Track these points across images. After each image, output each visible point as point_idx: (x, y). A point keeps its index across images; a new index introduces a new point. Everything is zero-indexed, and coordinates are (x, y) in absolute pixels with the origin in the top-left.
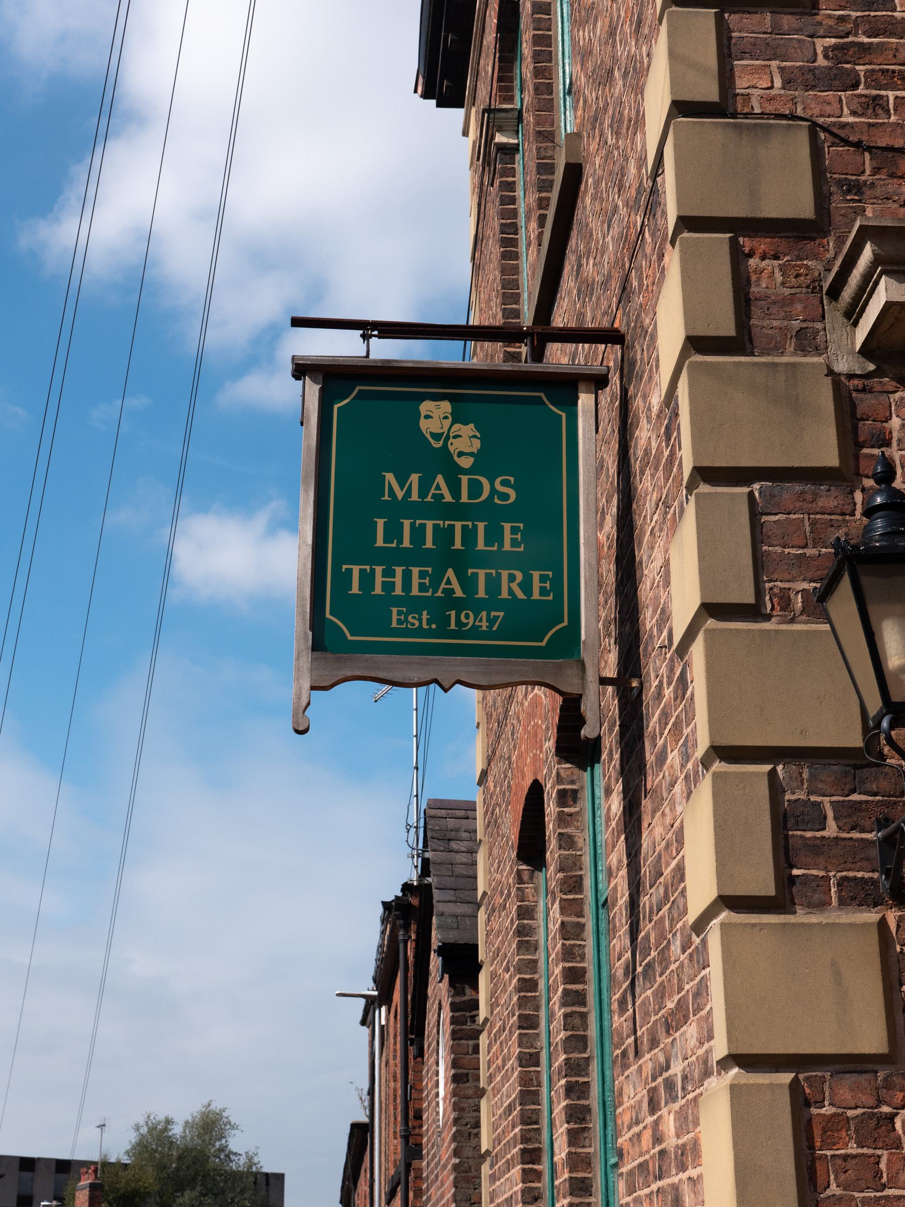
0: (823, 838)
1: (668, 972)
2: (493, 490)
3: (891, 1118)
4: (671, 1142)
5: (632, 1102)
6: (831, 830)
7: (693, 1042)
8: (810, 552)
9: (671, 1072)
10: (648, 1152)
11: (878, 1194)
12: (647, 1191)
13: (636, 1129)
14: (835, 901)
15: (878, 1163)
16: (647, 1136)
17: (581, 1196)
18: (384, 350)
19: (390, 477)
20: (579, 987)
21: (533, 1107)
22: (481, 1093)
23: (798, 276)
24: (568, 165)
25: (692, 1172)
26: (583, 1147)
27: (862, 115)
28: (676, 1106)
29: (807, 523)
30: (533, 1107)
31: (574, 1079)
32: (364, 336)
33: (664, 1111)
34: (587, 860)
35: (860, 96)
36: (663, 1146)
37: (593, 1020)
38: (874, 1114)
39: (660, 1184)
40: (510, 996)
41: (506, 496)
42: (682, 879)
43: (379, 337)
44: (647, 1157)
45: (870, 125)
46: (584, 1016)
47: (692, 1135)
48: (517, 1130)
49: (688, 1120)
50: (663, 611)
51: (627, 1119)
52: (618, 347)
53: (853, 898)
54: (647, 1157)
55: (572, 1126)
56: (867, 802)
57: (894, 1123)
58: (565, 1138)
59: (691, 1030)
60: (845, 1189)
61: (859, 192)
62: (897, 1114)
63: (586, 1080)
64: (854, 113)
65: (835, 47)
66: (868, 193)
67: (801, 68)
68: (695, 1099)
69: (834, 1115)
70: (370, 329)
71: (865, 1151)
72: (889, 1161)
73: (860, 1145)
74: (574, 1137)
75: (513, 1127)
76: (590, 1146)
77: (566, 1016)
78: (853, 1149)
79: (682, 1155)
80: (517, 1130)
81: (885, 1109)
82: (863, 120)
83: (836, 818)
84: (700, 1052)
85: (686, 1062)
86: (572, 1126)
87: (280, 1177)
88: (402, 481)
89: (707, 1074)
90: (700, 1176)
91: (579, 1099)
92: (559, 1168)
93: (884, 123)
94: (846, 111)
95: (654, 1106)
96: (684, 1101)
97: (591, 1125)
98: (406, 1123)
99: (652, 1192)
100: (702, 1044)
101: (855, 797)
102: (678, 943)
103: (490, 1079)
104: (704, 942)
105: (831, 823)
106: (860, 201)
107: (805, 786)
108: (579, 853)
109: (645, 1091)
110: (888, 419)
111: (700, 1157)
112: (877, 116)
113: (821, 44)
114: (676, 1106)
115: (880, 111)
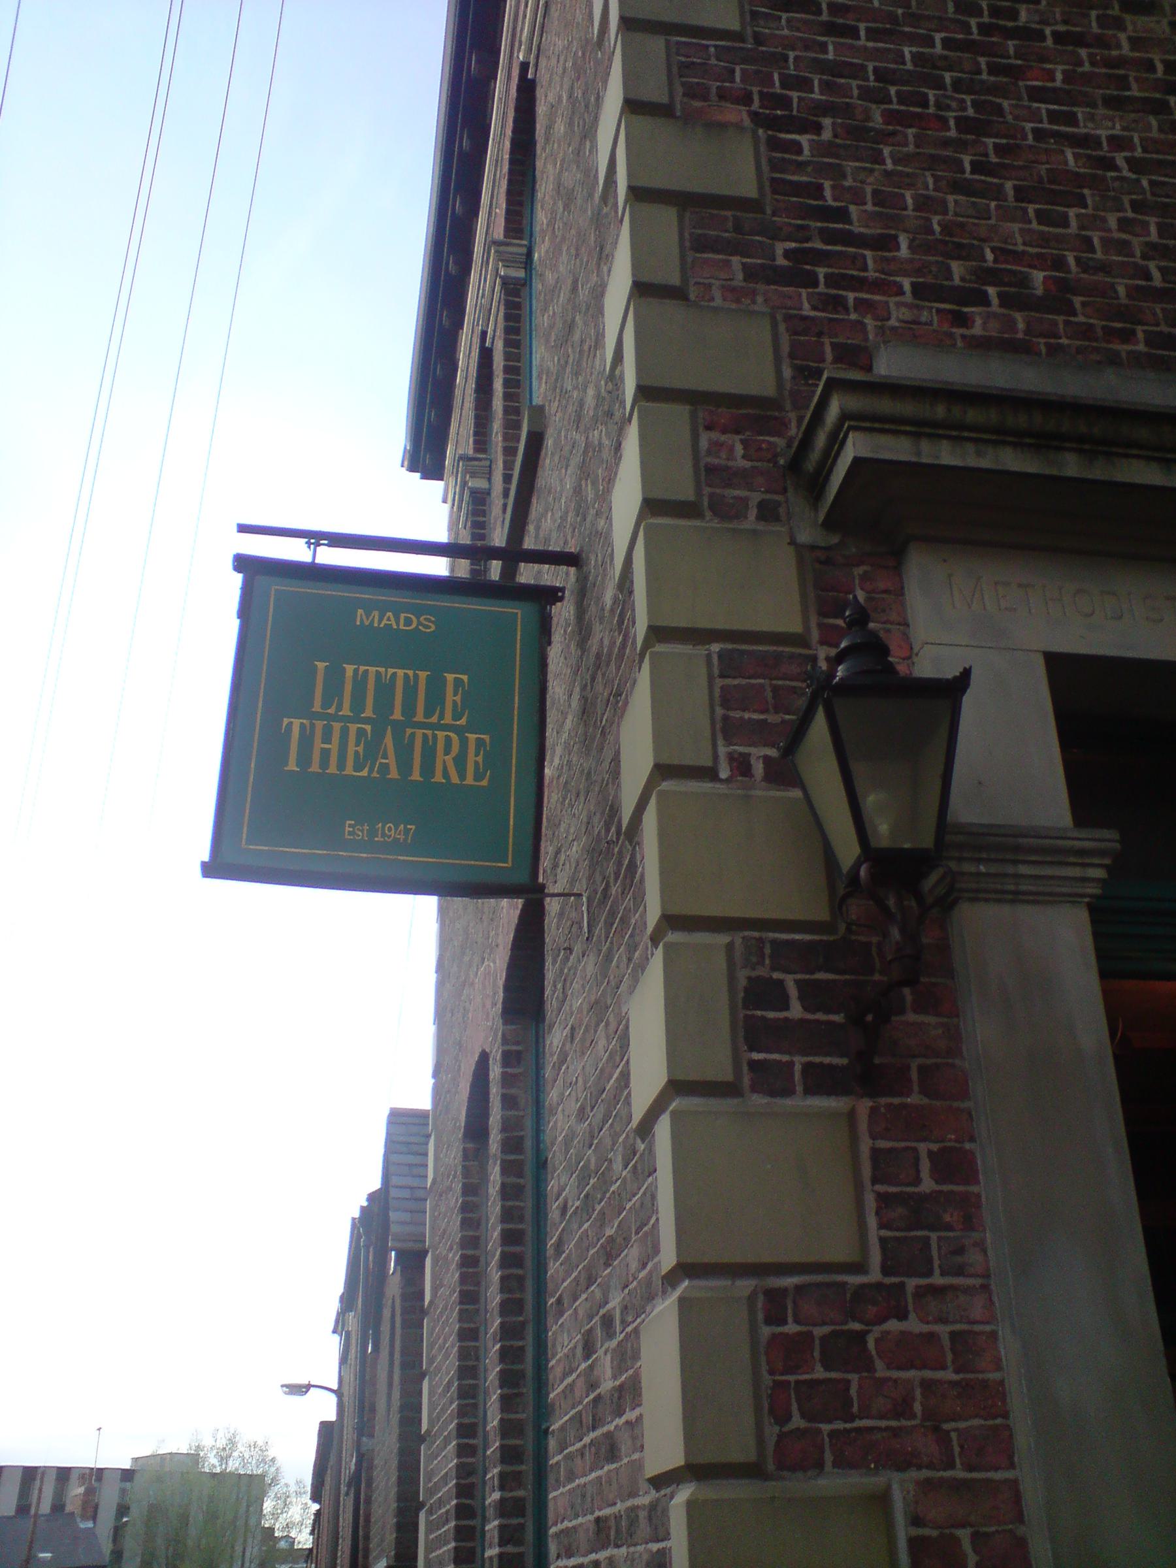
0: (786, 1019)
1: (608, 1195)
2: (419, 623)
3: (861, 1336)
4: (607, 1385)
5: (566, 1350)
6: (796, 1011)
7: (634, 1265)
8: (772, 718)
9: (609, 1306)
10: (580, 1403)
11: (848, 1426)
12: (579, 1445)
13: (569, 1380)
15: (848, 1389)
16: (580, 1385)
17: (512, 1464)
18: (330, 556)
20: (517, 1249)
21: (472, 1382)
22: (423, 1375)
24: (530, 433)
25: (630, 1415)
26: (517, 1412)
27: (823, 311)
28: (613, 1343)
29: (769, 689)
30: (472, 1382)
31: (508, 1343)
32: (309, 544)
33: (601, 1352)
34: (529, 1123)
35: (820, 294)
36: (598, 1391)
37: (529, 1284)
38: (843, 1332)
39: (592, 1435)
40: (453, 1276)
41: (428, 627)
42: (627, 1085)
43: (328, 545)
44: (580, 1407)
45: (831, 320)
46: (521, 1279)
47: (631, 1372)
48: (454, 1406)
49: (627, 1356)
50: (612, 807)
51: (558, 1371)
52: (572, 570)
54: (580, 1407)
55: (506, 1391)
56: (834, 981)
57: (865, 1343)
58: (497, 1405)
59: (632, 1254)
60: (809, 1421)
62: (868, 1332)
63: (520, 1343)
64: (814, 308)
65: (795, 250)
67: (762, 265)
68: (636, 1331)
69: (799, 1334)
70: (315, 538)
71: (833, 1375)
72: (860, 1387)
73: (827, 1368)
74: (507, 1402)
75: (451, 1403)
76: (523, 1412)
77: (502, 1278)
78: (820, 1373)
79: (619, 1398)
80: (454, 1406)
81: (856, 1326)
82: (823, 314)
83: (800, 998)
84: (642, 1274)
85: (626, 1291)
86: (506, 1391)
89: (650, 1298)
90: (640, 1418)
91: (513, 1363)
92: (491, 1436)
93: (843, 320)
95: (589, 1349)
96: (622, 1336)
97: (525, 1391)
98: (361, 1417)
99: (585, 1446)
100: (644, 1265)
101: (820, 976)
102: (620, 1158)
103: (431, 1361)
104: (650, 1149)
107: (767, 961)
108: (521, 1113)
109: (579, 1336)
111: (640, 1395)
112: (837, 312)
113: (780, 248)
114: (613, 1343)
115: (840, 309)
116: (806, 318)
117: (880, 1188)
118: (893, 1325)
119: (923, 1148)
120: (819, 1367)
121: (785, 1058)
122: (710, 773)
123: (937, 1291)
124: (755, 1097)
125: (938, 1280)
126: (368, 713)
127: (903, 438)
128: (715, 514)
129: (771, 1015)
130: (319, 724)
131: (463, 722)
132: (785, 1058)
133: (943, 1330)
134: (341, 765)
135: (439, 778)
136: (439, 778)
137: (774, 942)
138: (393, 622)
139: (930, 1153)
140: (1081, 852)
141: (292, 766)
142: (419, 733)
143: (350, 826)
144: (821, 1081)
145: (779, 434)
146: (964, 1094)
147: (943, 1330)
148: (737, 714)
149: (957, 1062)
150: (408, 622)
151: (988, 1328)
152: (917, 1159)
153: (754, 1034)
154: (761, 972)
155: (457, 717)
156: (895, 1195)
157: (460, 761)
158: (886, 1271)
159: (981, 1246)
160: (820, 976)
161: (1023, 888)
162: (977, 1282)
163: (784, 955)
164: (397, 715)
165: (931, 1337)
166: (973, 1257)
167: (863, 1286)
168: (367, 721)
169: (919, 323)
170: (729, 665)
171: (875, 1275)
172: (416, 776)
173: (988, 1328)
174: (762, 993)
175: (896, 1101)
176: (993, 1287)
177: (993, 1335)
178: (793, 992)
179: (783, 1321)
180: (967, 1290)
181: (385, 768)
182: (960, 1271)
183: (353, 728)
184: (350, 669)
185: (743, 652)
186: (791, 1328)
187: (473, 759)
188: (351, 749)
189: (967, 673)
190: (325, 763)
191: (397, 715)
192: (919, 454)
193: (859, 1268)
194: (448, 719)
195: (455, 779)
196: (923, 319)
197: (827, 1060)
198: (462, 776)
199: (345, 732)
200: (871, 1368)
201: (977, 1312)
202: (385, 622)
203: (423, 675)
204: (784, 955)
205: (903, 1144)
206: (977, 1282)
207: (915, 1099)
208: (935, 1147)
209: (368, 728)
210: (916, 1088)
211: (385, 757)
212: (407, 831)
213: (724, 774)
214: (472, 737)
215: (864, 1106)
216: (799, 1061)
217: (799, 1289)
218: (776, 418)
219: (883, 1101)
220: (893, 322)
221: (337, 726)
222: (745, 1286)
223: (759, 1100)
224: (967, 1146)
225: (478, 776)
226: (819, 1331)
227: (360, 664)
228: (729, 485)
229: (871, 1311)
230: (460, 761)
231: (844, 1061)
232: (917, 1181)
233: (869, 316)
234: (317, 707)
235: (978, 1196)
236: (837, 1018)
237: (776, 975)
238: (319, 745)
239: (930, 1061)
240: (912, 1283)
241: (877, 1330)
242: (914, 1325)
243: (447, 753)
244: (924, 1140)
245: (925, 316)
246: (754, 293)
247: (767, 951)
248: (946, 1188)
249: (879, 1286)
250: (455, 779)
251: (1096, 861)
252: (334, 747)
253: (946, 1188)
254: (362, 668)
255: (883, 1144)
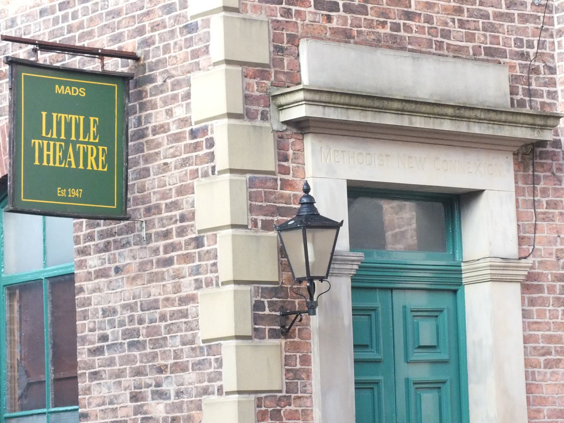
2: (79, 92)
3: (280, 410)
6: (267, 312)
14: (267, 336)
19: (57, 86)
23: (262, 87)
41: (82, 94)
45: (287, 22)
53: (273, 336)
61: (283, 52)
66: (286, 52)
73: (272, 420)
81: (279, 408)
83: (268, 307)
87: (349, 182)
88: (60, 88)
94: (279, 15)
101: (274, 299)
105: (267, 309)
106: (282, 56)
110: (288, 150)
116: (278, 21)
117: (287, 367)
118: (288, 407)
119: (298, 355)
120: (269, 420)
121: (264, 327)
122: (245, 227)
123: (299, 398)
124: (256, 339)
125: (299, 394)
126: (63, 137)
127: (320, 107)
128: (248, 118)
129: (260, 313)
130: (45, 142)
131: (97, 141)
132: (264, 327)
133: (300, 409)
134: (55, 162)
135: (89, 168)
136: (89, 168)
137: (262, 288)
138: (69, 92)
139: (300, 356)
140: (353, 261)
141: (37, 163)
142: (82, 146)
143: (60, 190)
144: (274, 334)
145: (269, 80)
146: (310, 338)
147: (300, 409)
148: (254, 203)
149: (308, 327)
150: (75, 92)
151: (311, 408)
152: (296, 358)
153: (256, 319)
154: (259, 298)
155: (95, 138)
156: (290, 369)
157: (97, 159)
158: (287, 392)
159: (310, 384)
160: (274, 299)
161: (334, 272)
162: (309, 395)
163: (266, 292)
164: (73, 138)
165: (297, 411)
166: (308, 388)
167: (281, 396)
168: (62, 140)
169: (315, 22)
170: (252, 183)
171: (284, 394)
172: (81, 167)
173: (311, 408)
174: (258, 306)
175: (292, 340)
176: (313, 396)
177: (312, 410)
178: (266, 305)
179: (261, 407)
180: (307, 398)
181: (70, 163)
182: (305, 392)
183: (58, 144)
184: (55, 115)
185: (256, 178)
186: (263, 408)
187: (101, 158)
188: (58, 154)
189: (342, 221)
190: (48, 162)
191: (73, 138)
192: (324, 114)
193: (280, 391)
194: (92, 140)
195: (95, 168)
196: (317, 20)
197: (274, 327)
198: (98, 167)
199: (55, 145)
200: (282, 420)
201: (308, 404)
202: (66, 91)
203: (82, 118)
204: (266, 292)
205: (293, 354)
206: (309, 395)
207: (297, 339)
208: (301, 354)
209: (63, 144)
210: (297, 336)
211: (70, 158)
212: (79, 192)
213: (250, 227)
214: (101, 148)
215: (283, 341)
216: (267, 328)
217: (265, 397)
218: (267, 71)
219: (288, 340)
220: (307, 22)
221: (52, 143)
222: (253, 397)
223: (256, 340)
224: (309, 354)
225: (103, 167)
226: (270, 409)
227: (58, 113)
228: (252, 104)
229: (283, 404)
230: (97, 159)
231: (279, 328)
232: (296, 365)
233: (299, 19)
234: (44, 134)
235: (311, 369)
236: (278, 313)
237: (262, 300)
238: (45, 153)
239: (301, 327)
240: (293, 395)
241: (284, 409)
242: (293, 407)
243: (92, 156)
244: (298, 352)
245: (318, 18)
246: (261, 8)
247: (260, 291)
248: (303, 367)
249: (285, 396)
250: (95, 168)
251: (356, 263)
252: (51, 153)
253: (303, 367)
254: (59, 115)
255: (288, 354)
